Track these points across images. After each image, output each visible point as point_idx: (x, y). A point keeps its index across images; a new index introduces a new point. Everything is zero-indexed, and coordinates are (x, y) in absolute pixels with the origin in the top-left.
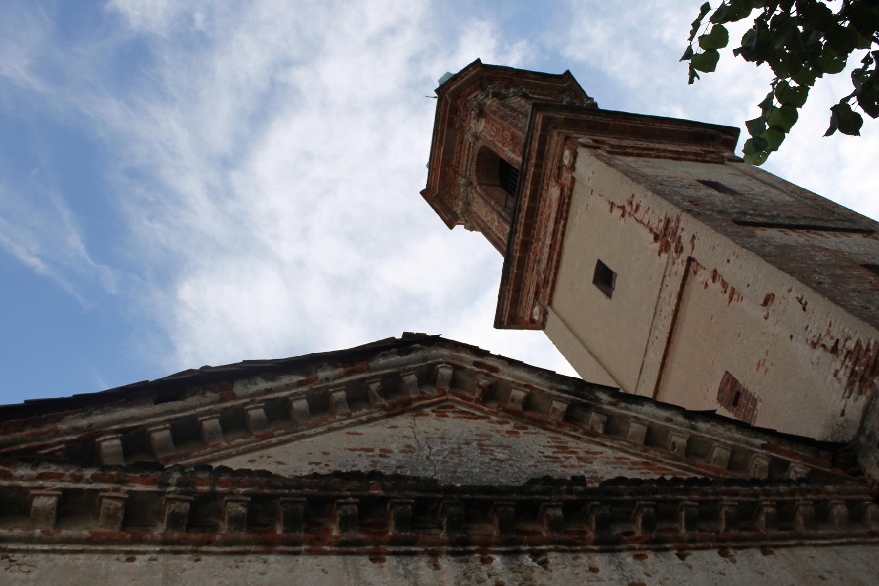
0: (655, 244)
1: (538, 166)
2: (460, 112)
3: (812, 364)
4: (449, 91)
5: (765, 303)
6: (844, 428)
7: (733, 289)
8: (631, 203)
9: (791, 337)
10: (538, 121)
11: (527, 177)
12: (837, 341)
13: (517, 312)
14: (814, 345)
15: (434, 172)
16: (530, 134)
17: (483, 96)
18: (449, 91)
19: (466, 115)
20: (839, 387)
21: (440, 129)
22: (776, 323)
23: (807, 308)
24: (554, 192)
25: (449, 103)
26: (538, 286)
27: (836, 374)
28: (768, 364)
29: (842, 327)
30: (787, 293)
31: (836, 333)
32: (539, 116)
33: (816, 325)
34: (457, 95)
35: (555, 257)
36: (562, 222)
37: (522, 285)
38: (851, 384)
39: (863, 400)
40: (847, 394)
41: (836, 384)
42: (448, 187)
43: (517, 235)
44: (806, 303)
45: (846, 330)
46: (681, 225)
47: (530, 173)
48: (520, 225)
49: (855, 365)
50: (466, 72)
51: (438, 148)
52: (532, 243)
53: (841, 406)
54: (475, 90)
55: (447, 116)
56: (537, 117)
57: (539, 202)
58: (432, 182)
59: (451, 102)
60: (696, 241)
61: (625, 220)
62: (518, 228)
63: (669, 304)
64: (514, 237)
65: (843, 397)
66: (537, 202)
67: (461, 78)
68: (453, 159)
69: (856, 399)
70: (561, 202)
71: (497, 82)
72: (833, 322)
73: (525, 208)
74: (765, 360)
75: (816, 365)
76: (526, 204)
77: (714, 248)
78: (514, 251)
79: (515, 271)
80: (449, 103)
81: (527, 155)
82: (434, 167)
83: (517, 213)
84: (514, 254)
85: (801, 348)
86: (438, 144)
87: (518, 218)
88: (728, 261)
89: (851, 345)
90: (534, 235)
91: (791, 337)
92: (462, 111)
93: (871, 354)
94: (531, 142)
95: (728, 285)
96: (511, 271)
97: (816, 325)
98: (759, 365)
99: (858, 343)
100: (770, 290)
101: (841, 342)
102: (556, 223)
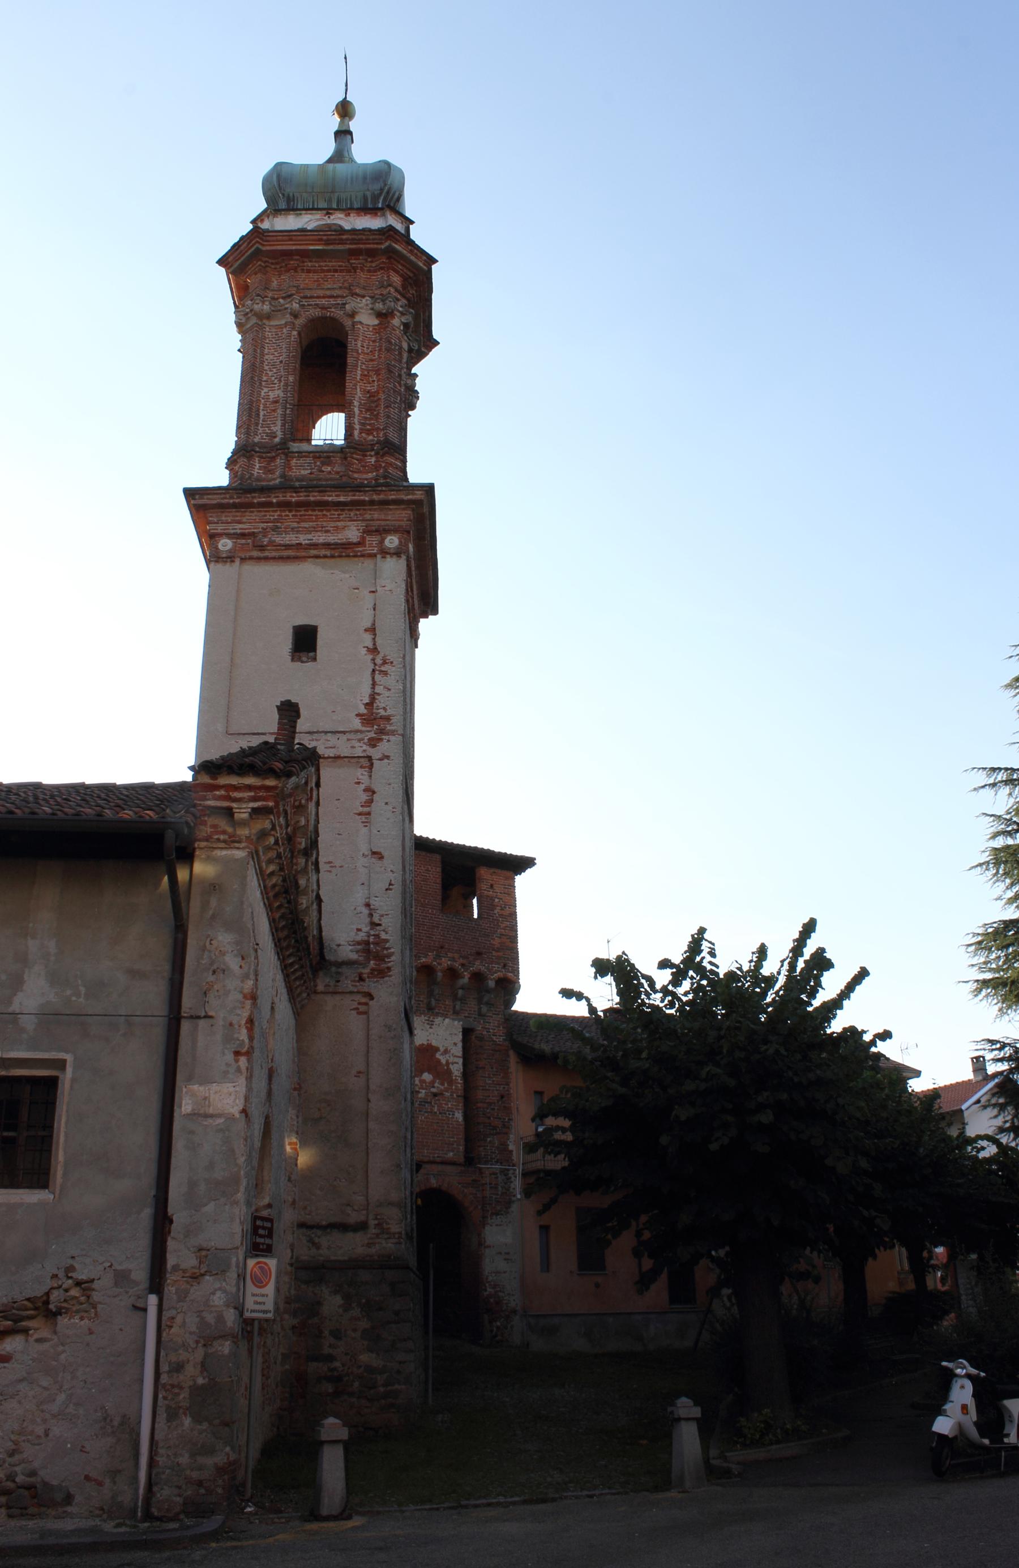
0: (363, 707)
1: (372, 502)
2: (372, 262)
3: (355, 909)
4: (394, 245)
5: (374, 853)
6: (330, 951)
7: (369, 814)
8: (385, 663)
9: (363, 884)
10: (415, 494)
11: (357, 493)
12: (380, 925)
13: (211, 511)
14: (368, 905)
15: (287, 238)
16: (401, 488)
17: (401, 309)
18: (394, 245)
19: (369, 271)
20: (353, 936)
21: (344, 237)
22: (364, 867)
23: (389, 891)
24: (352, 533)
25: (379, 246)
26: (252, 535)
27: (359, 930)
28: (333, 870)
29: (390, 924)
30: (389, 870)
31: (385, 921)
32: (422, 494)
33: (382, 904)
34: (391, 253)
35: (290, 553)
36: (328, 553)
37: (243, 510)
38: (359, 943)
39: (354, 956)
40: (352, 943)
41: (353, 934)
42: (274, 261)
43: (294, 495)
44: (391, 889)
45: (390, 929)
46: (392, 738)
47: (362, 496)
48: (306, 496)
49: (373, 943)
50: (419, 254)
51: (321, 240)
52: (290, 511)
53: (342, 943)
54: (401, 276)
55: (361, 246)
56: (420, 492)
57: (336, 510)
58: (275, 238)
59: (381, 249)
60: (386, 761)
61: (366, 654)
62: (301, 494)
63: (326, 748)
64: (291, 492)
65: (348, 942)
66: (335, 508)
67: (411, 252)
68: (310, 261)
69: (351, 951)
70: (347, 546)
71: (414, 292)
72: (390, 916)
73: (326, 498)
74: (335, 866)
75: (356, 912)
76: (330, 499)
77: (389, 784)
78: (277, 495)
79: (255, 501)
80: (379, 246)
81: (380, 489)
82: (294, 238)
83: (317, 489)
84: (273, 495)
85: (359, 897)
86: (325, 238)
87: (312, 491)
88: (386, 803)
89: (383, 936)
90: (300, 511)
91: (363, 884)
92: (374, 265)
93: (385, 952)
94: (393, 490)
95: (369, 806)
96: (253, 495)
97: (382, 904)
98: (330, 862)
99: (387, 941)
100: (385, 854)
101: (382, 928)
102: (327, 545)
